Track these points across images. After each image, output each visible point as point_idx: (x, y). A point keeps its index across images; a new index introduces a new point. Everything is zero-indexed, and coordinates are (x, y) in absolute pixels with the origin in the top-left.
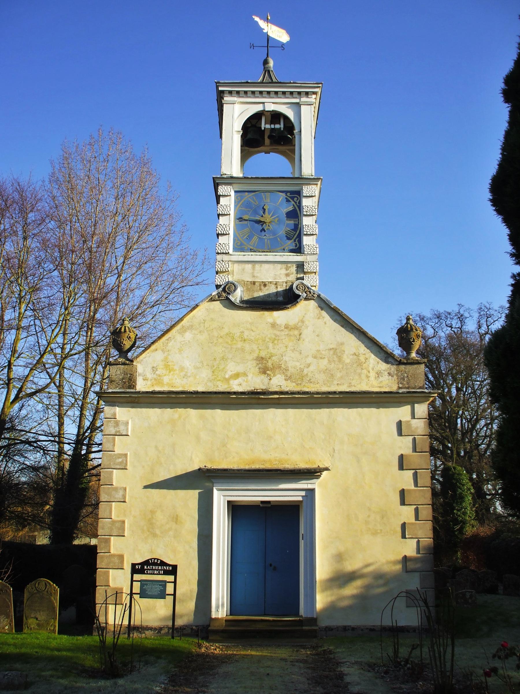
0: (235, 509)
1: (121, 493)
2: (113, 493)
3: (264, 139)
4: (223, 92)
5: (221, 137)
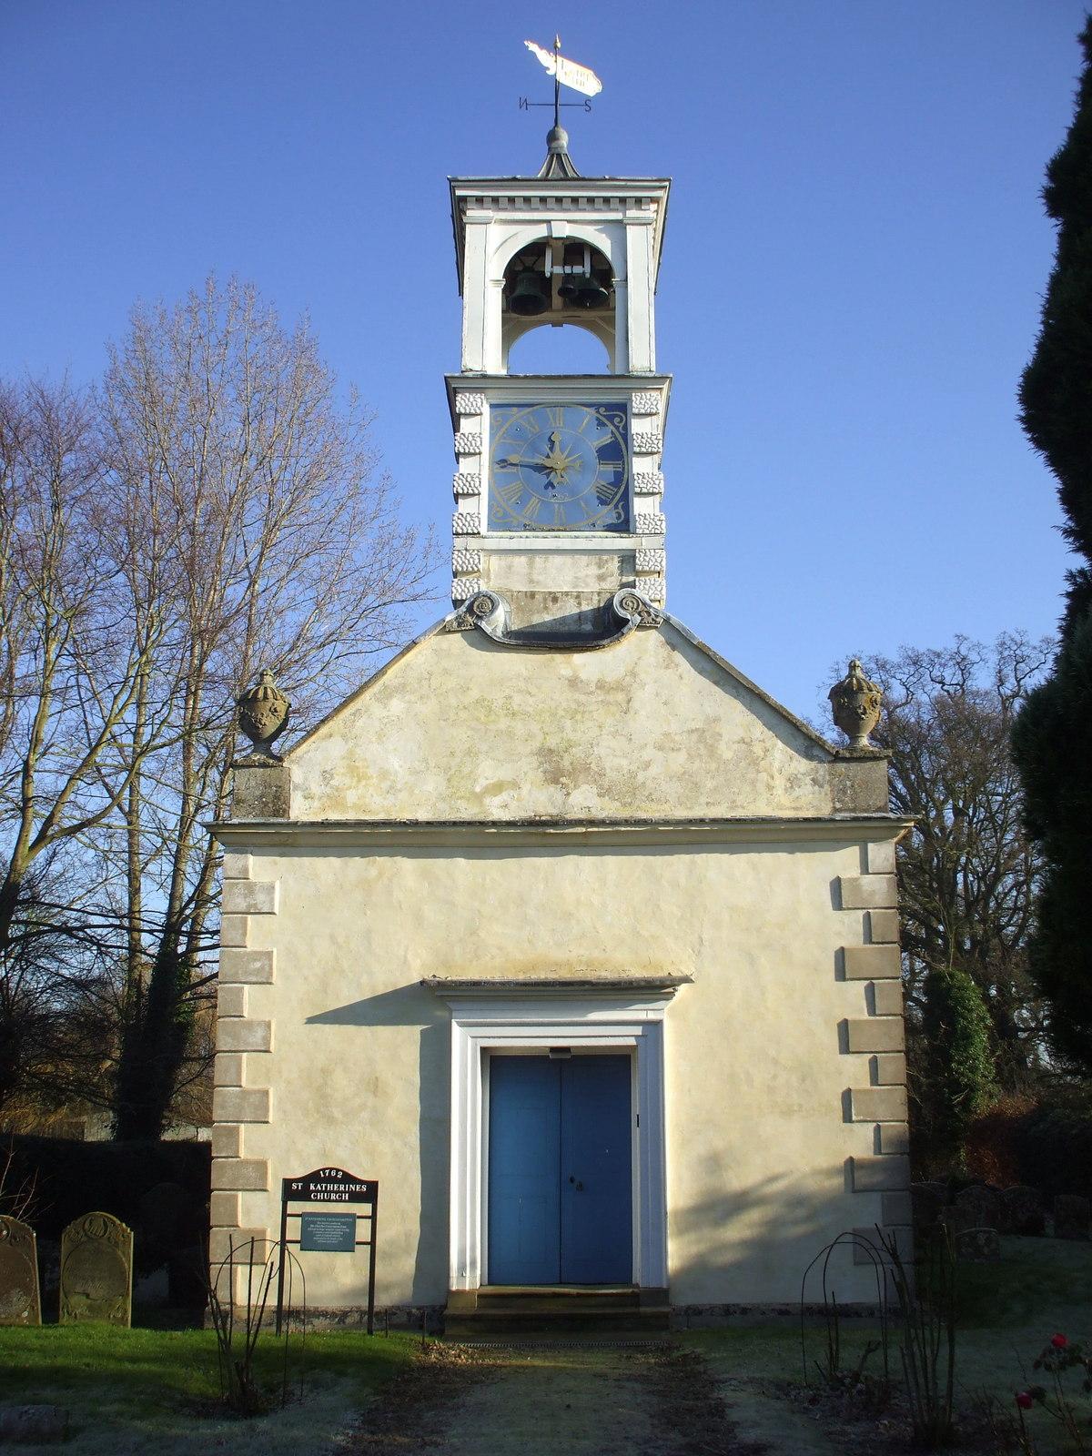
0: (497, 1064)
1: (260, 1033)
2: (244, 1032)
3: (550, 296)
4: (464, 199)
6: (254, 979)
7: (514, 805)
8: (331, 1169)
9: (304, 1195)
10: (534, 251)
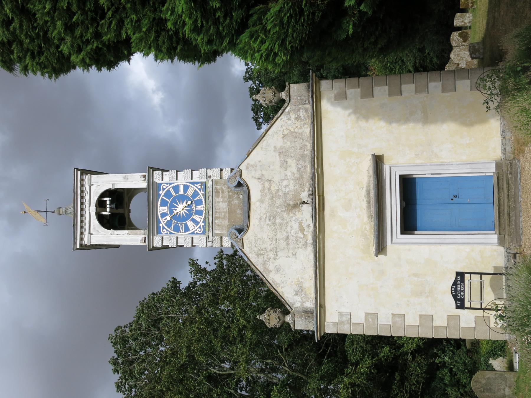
1: (397, 319)
3: (119, 214)
4: (81, 245)
6: (376, 321)
7: (308, 223)
8: (451, 290)
9: (462, 301)
10: (101, 219)
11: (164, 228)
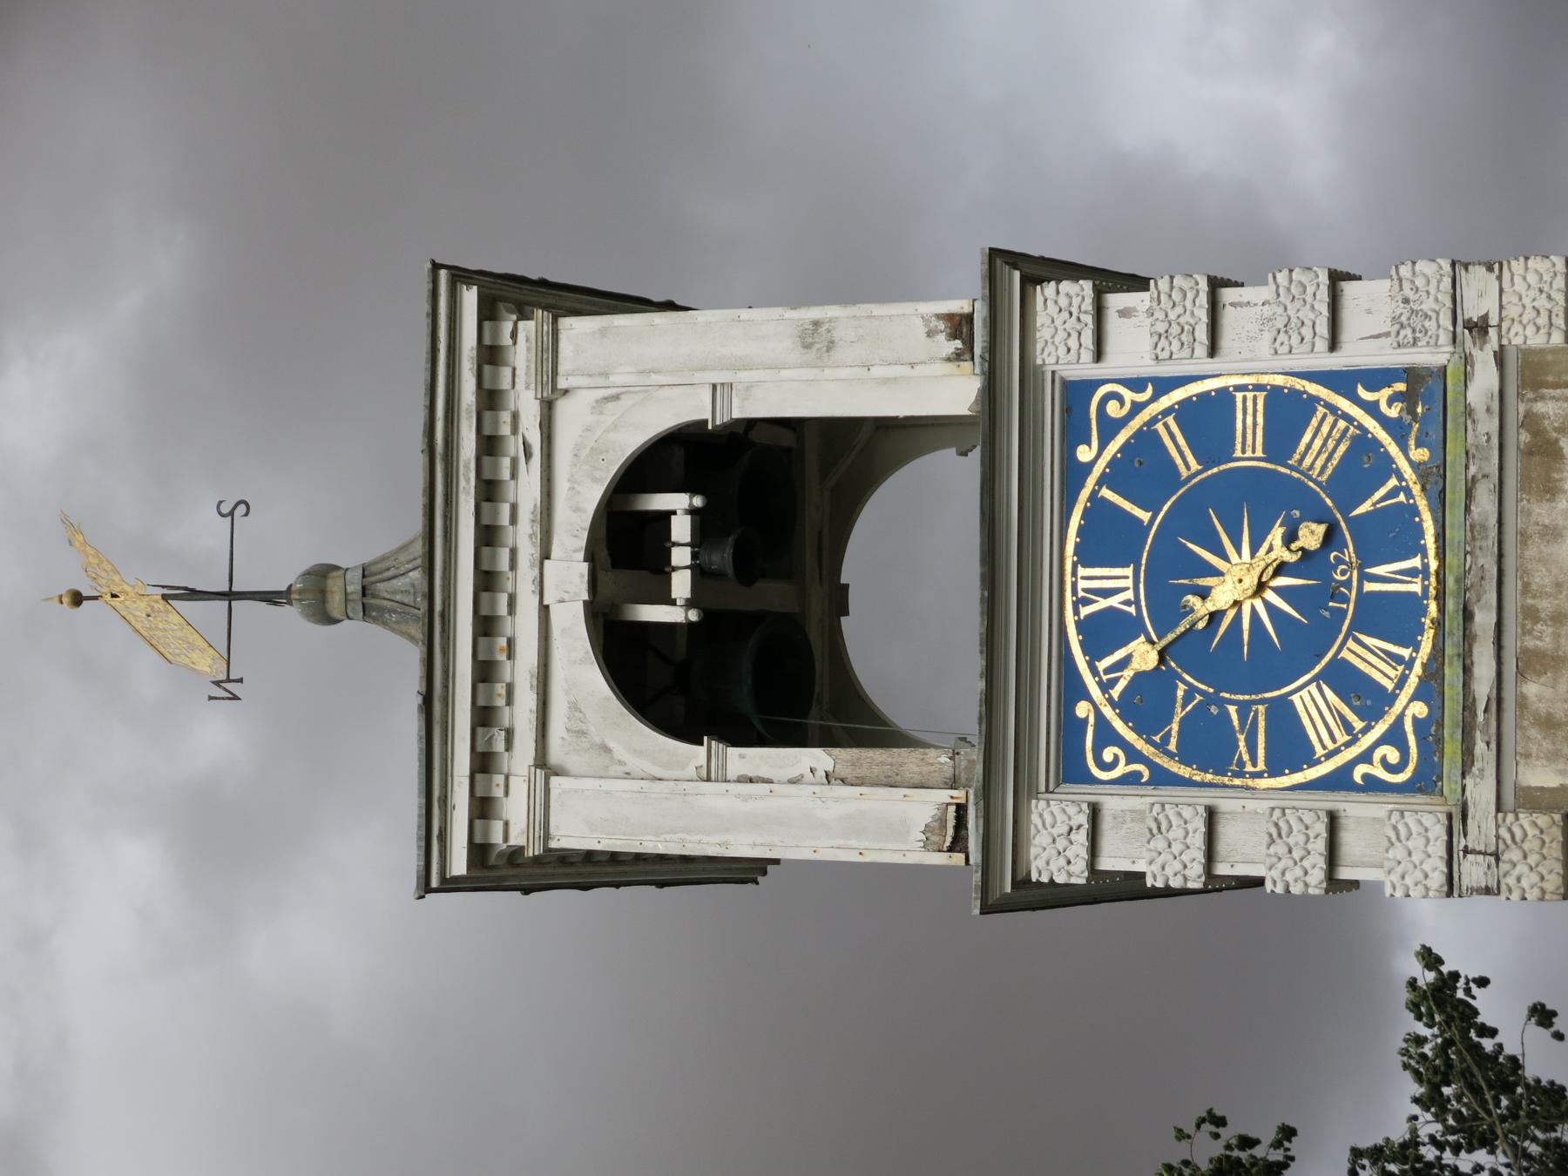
3: (758, 617)
4: (479, 851)
5: (748, 871)
11: (1106, 735)
